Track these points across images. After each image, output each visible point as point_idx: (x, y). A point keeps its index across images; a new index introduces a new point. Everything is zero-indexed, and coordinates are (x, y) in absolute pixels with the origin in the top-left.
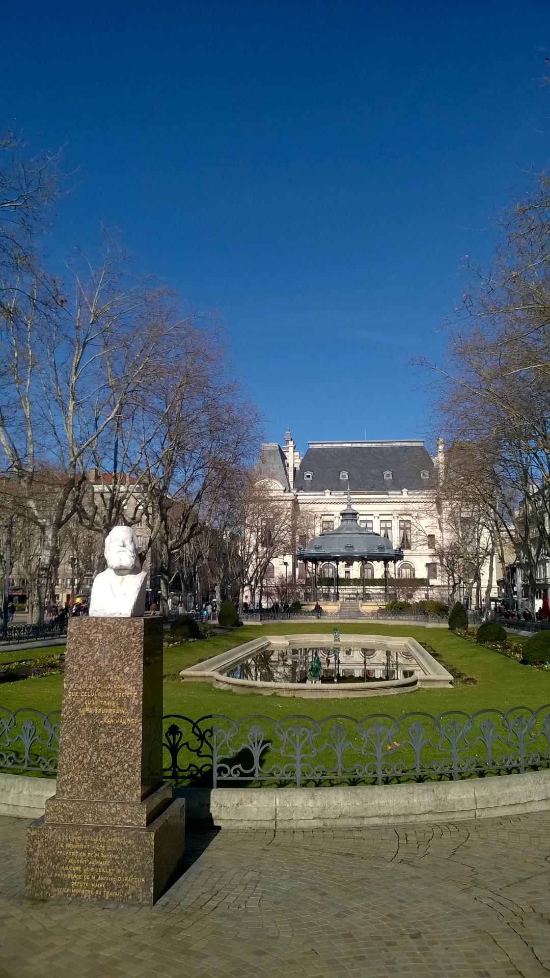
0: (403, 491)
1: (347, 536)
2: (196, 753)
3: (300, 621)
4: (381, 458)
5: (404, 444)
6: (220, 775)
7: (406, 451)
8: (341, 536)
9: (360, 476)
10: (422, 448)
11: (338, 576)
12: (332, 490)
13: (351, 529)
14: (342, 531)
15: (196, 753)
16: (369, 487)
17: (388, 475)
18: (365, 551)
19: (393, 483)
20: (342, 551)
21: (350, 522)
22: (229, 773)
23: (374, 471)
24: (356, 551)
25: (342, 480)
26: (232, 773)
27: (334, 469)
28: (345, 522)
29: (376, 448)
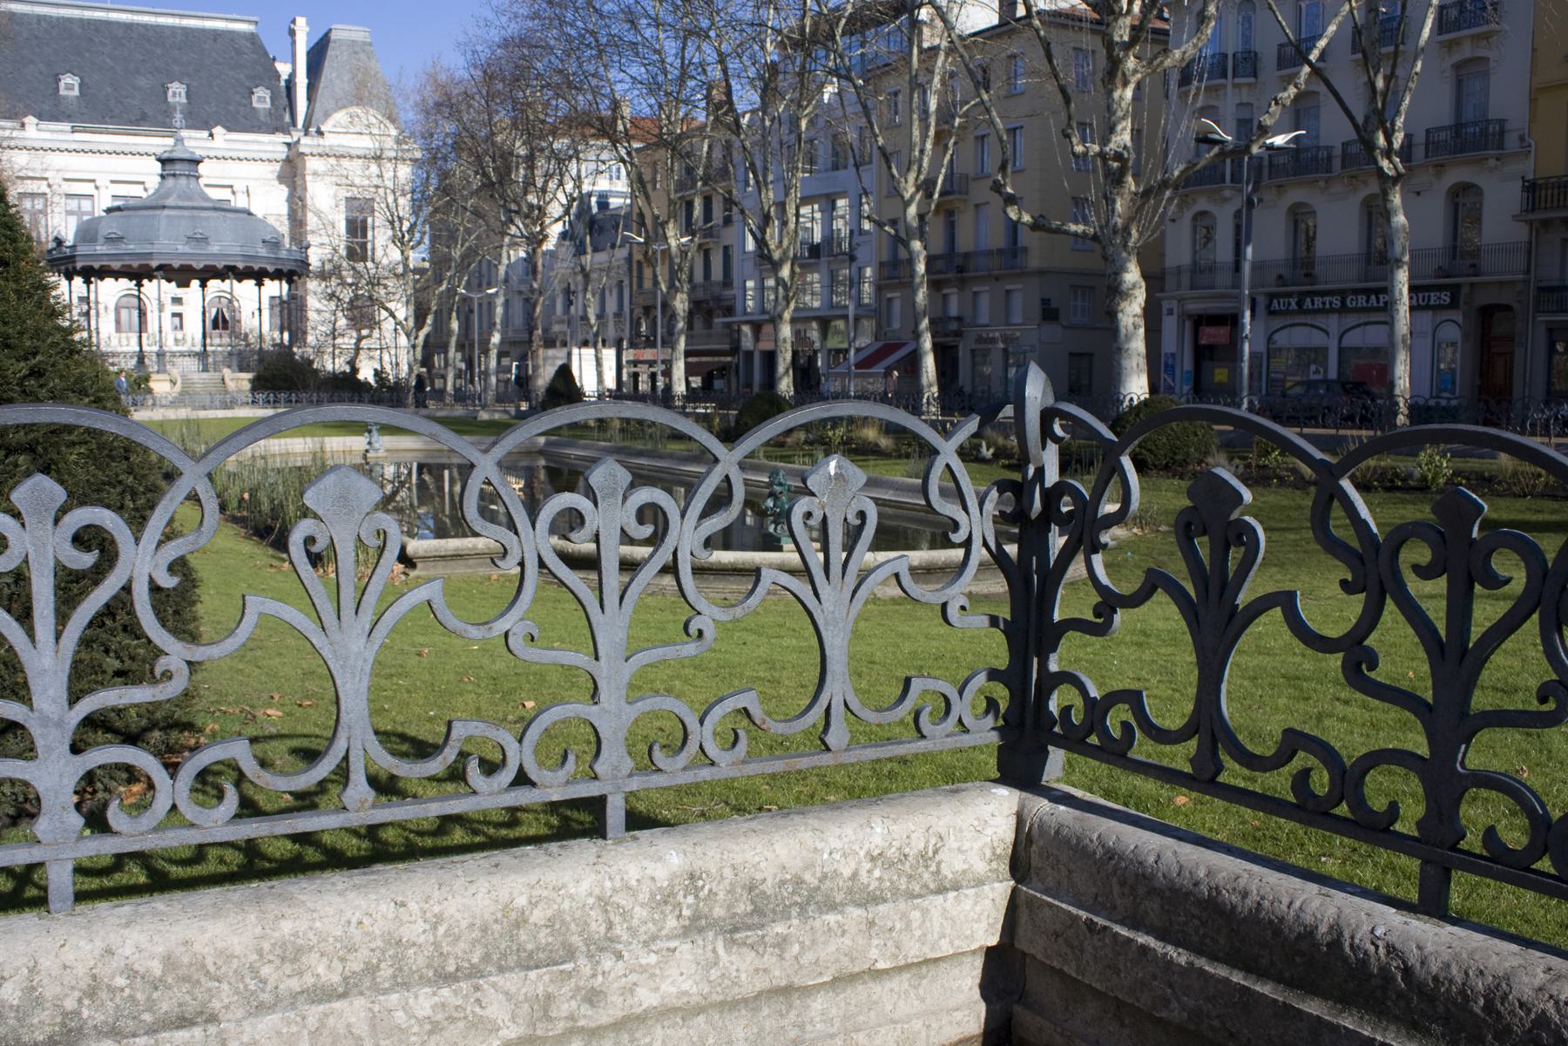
0: (214, 131)
1: (186, 213)
2: (1335, 661)
3: (1246, 371)
4: (159, 51)
5: (209, 24)
6: (97, 822)
7: (215, 40)
8: (172, 213)
9: (109, 90)
10: (253, 38)
11: (1000, 251)
12: (40, 117)
13: (189, 198)
14: (170, 202)
15: (1335, 661)
16: (133, 118)
17: (177, 92)
18: (237, 250)
19: (190, 113)
20: (182, 248)
21: (183, 181)
22: (161, 804)
23: (142, 82)
24: (215, 248)
25: (65, 98)
26: (712, 750)
27: (42, 67)
28: (170, 182)
29: (146, 26)
